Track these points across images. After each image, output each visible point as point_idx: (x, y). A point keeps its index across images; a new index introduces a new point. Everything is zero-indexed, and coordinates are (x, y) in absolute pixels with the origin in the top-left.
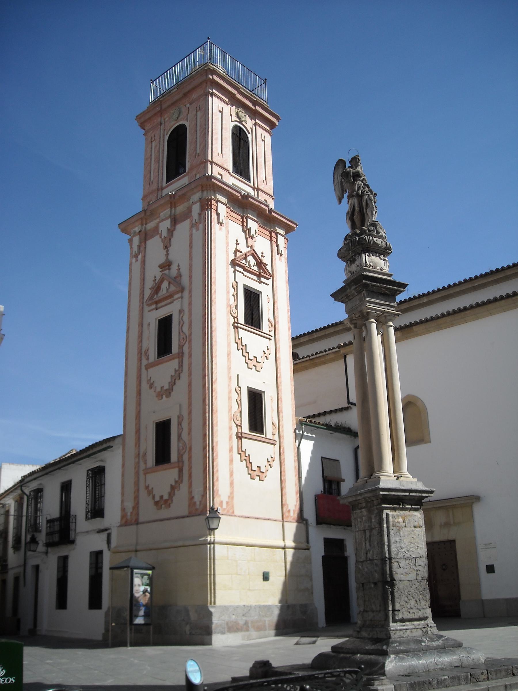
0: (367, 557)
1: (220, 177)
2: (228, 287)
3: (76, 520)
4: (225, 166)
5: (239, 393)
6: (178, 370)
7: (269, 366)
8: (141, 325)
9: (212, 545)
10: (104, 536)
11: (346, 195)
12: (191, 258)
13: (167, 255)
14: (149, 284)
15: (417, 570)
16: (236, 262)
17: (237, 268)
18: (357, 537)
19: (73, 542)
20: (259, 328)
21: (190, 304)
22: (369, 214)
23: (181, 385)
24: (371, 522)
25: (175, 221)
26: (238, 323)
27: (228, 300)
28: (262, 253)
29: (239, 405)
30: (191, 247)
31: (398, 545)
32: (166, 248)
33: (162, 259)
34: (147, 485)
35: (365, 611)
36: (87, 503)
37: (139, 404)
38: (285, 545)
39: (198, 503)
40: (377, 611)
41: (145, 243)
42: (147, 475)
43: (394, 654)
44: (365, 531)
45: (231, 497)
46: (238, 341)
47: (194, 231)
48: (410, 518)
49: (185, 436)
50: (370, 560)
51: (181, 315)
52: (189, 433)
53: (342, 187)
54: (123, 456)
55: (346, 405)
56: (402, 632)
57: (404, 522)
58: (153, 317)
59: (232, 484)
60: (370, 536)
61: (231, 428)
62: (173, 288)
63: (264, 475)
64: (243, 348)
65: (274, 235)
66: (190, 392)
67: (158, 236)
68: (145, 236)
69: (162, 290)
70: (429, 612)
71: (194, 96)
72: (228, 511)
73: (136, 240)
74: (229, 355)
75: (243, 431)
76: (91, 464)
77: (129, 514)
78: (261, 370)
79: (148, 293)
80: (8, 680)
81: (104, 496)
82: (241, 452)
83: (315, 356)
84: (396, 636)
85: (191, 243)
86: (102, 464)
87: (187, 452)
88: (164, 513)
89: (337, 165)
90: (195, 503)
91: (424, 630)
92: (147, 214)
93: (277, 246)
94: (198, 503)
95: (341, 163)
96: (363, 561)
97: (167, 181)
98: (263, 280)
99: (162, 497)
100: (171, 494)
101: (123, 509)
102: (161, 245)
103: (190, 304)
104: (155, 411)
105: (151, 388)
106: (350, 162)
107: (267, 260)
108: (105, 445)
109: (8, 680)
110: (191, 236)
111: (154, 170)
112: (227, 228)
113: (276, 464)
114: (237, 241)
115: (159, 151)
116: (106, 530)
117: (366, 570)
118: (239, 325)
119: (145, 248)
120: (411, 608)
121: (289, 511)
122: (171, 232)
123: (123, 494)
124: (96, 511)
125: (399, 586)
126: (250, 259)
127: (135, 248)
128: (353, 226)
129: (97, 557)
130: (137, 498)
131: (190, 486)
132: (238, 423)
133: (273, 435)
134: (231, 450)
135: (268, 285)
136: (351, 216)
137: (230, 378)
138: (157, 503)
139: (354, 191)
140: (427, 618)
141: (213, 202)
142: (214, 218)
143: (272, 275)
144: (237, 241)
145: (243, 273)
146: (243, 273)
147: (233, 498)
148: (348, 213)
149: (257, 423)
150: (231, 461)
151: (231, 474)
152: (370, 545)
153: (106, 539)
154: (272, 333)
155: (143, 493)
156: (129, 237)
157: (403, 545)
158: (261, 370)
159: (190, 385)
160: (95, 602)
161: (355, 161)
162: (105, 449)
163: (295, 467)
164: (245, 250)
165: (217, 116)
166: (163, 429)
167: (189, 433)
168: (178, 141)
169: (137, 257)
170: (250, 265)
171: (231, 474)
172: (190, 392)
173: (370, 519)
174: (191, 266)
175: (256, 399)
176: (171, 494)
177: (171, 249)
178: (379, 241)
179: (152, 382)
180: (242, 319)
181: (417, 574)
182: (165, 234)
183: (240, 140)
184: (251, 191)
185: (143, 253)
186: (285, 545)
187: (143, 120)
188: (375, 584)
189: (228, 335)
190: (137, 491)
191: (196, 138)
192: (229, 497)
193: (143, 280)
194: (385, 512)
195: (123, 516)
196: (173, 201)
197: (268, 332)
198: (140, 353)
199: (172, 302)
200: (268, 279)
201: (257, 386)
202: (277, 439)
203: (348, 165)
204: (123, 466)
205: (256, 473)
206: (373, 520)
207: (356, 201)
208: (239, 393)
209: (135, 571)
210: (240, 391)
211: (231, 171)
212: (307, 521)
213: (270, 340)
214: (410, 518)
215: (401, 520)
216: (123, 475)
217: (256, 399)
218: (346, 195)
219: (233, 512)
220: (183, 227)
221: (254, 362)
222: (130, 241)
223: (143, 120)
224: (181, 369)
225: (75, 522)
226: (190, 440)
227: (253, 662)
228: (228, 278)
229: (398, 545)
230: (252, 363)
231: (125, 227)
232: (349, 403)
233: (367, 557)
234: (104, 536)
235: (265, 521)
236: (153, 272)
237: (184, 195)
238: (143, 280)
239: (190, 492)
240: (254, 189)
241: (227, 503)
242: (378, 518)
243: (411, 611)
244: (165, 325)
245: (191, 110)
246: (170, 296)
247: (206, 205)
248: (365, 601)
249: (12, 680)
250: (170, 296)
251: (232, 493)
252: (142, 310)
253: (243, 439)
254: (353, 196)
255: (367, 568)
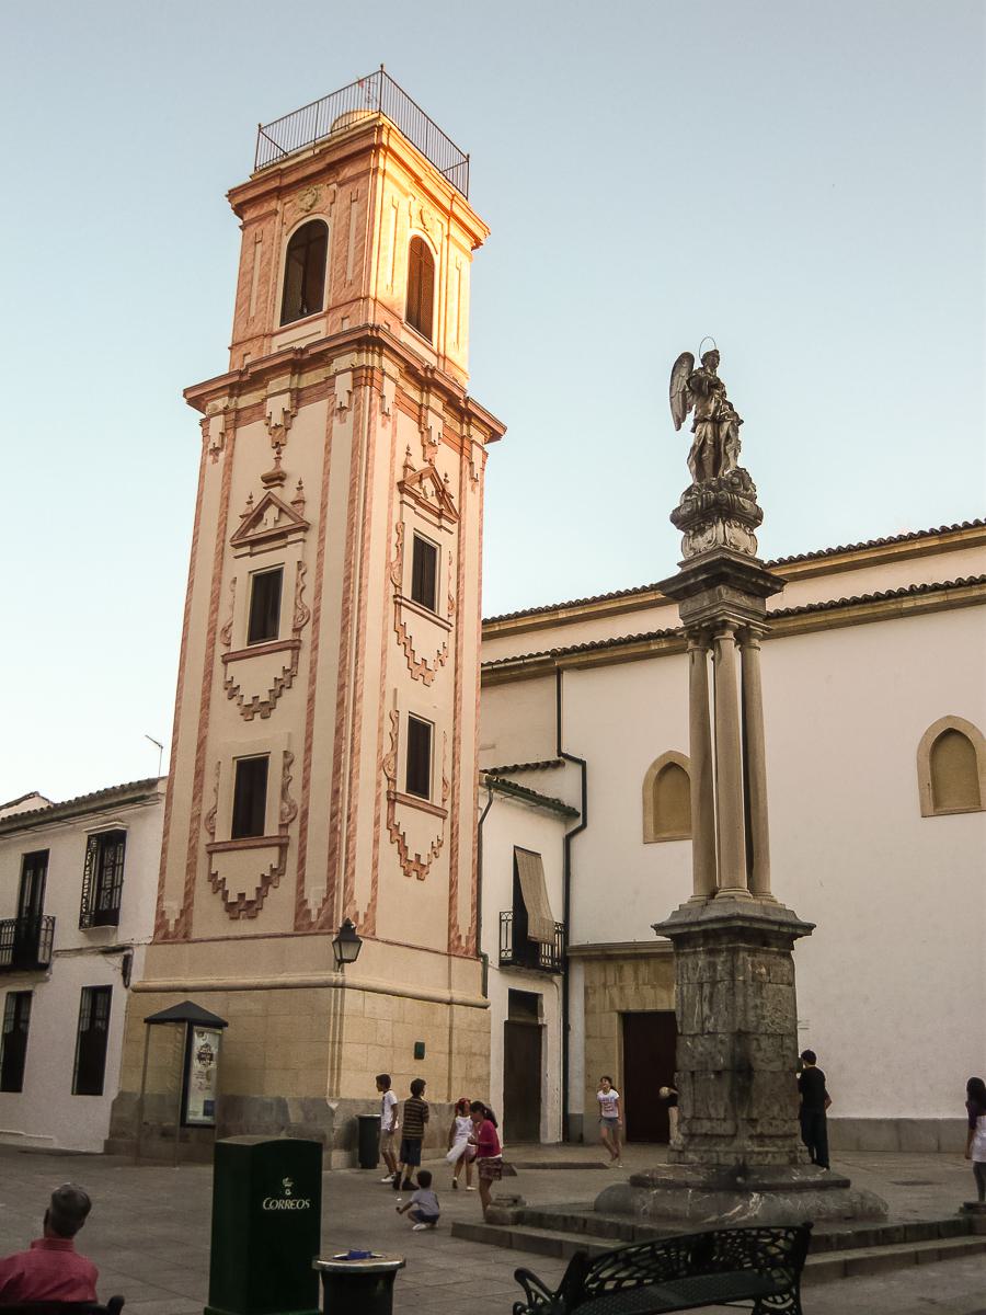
0: (703, 1029)
1: (387, 327)
2: (389, 532)
3: (53, 925)
4: (397, 312)
5: (394, 720)
6: (289, 670)
7: (444, 676)
8: (217, 580)
9: (340, 990)
10: (117, 960)
11: (691, 417)
12: (327, 473)
13: (278, 459)
14: (239, 507)
15: (783, 1056)
16: (406, 487)
17: (407, 498)
18: (685, 993)
19: (46, 967)
20: (433, 609)
21: (320, 554)
22: (731, 454)
23: (294, 699)
24: (715, 970)
25: (299, 397)
26: (401, 597)
27: (389, 554)
28: (446, 476)
29: (394, 745)
30: (328, 451)
31: (759, 1011)
32: (277, 445)
33: (268, 468)
34: (213, 872)
35: (695, 1118)
36: (83, 897)
37: (204, 723)
38: (452, 998)
39: (314, 913)
40: (718, 1119)
41: (235, 431)
42: (215, 856)
43: (756, 1191)
44: (701, 985)
45: (372, 906)
46: (400, 629)
47: (336, 421)
48: (777, 969)
49: (295, 792)
50: (709, 1033)
51: (302, 571)
52: (305, 785)
53: (684, 400)
54: (167, 817)
55: (556, 758)
56: (760, 1157)
57: (768, 974)
58: (243, 569)
59: (375, 882)
60: (711, 995)
61: (379, 784)
62: (286, 522)
63: (426, 869)
64: (406, 643)
65: (466, 443)
66: (310, 713)
67: (262, 422)
68: (236, 418)
69: (264, 521)
70: (797, 1127)
71: (348, 172)
72: (366, 931)
73: (217, 424)
74: (384, 652)
75: (398, 791)
76: (97, 824)
77: (172, 922)
78: (432, 684)
79: (235, 524)
80: (301, 1204)
81: (120, 887)
82: (393, 828)
83: (503, 665)
84: (752, 1163)
85: (328, 445)
86: (120, 827)
87: (298, 818)
88: (244, 927)
89: (679, 362)
90: (309, 911)
91: (792, 1155)
92: (244, 381)
93: (471, 464)
94: (314, 913)
95: (687, 358)
96: (696, 1035)
97: (284, 321)
98: (444, 523)
99: (242, 896)
100: (261, 892)
101: (160, 914)
102: (268, 441)
103: (320, 554)
104: (237, 738)
105: (231, 697)
106: (703, 361)
107: (452, 488)
108: (138, 794)
109: (301, 1204)
110: (329, 431)
111: (258, 298)
112: (394, 423)
113: (445, 852)
114: (408, 448)
115: (269, 263)
116: (121, 949)
117: (700, 1049)
118: (403, 601)
119: (234, 440)
120: (774, 1118)
121: (460, 938)
122: (289, 415)
123: (161, 886)
124: (102, 913)
125: (759, 1079)
126: (427, 483)
127: (215, 439)
128: (699, 473)
129: (97, 998)
130: (188, 894)
131: (301, 880)
132: (390, 774)
133: (444, 800)
134: (377, 823)
135: (451, 533)
136: (698, 455)
137: (383, 694)
138: (230, 907)
139: (708, 411)
140: (795, 1135)
141: (377, 375)
142: (376, 405)
143: (459, 517)
144: (408, 448)
145: (414, 509)
146: (414, 509)
147: (375, 907)
148: (693, 448)
149: (419, 780)
150: (376, 842)
151: (375, 866)
152: (711, 1009)
153: (121, 965)
154: (452, 620)
155: (203, 888)
156: (203, 416)
157: (765, 1013)
158: (432, 684)
159: (311, 699)
160: (88, 1078)
161: (712, 358)
162: (133, 801)
163: (474, 861)
164: (419, 464)
165: (390, 214)
166: (252, 773)
167: (305, 785)
168: (308, 248)
169: (217, 455)
170: (425, 494)
171: (375, 866)
172: (310, 713)
173: (712, 966)
174: (326, 486)
175: (420, 733)
176: (261, 892)
177: (285, 451)
178: (747, 504)
179: (235, 686)
180: (407, 592)
181: (784, 1063)
182: (277, 419)
183: (421, 260)
184: (432, 361)
185: (230, 448)
186: (452, 998)
187: (245, 201)
188: (718, 1073)
189: (385, 617)
190: (190, 883)
191: (347, 251)
192: (369, 905)
193: (226, 499)
194: (741, 955)
195: (161, 925)
196: (299, 362)
197: (446, 619)
198: (212, 630)
199: (285, 546)
200: (453, 522)
201: (426, 713)
202: (449, 810)
203: (698, 365)
204: (166, 833)
205: (412, 866)
206: (719, 968)
207: (709, 428)
208: (394, 720)
209: (196, 1028)
210: (397, 718)
211: (403, 321)
212: (485, 957)
213: (449, 631)
214: (777, 969)
215: (764, 970)
216: (164, 851)
217: (420, 733)
218: (691, 417)
219: (374, 934)
220: (314, 414)
221: (423, 670)
222: (203, 422)
223: (245, 201)
224: (294, 669)
225: (53, 931)
226: (306, 799)
227: (47, 1204)
228: (390, 514)
229: (759, 1011)
230: (420, 671)
231: (197, 398)
232: (560, 753)
233: (703, 1029)
234: (117, 960)
235: (423, 953)
236: (248, 487)
237: (322, 354)
238: (226, 499)
239: (300, 892)
240: (438, 356)
241: (366, 916)
242: (729, 964)
243: (774, 1123)
244: (267, 588)
245: (339, 196)
246: (282, 535)
247: (363, 378)
248: (695, 1101)
249: (306, 1203)
250: (282, 535)
251: (374, 899)
252: (221, 553)
253: (397, 804)
254: (705, 420)
255: (702, 1046)
